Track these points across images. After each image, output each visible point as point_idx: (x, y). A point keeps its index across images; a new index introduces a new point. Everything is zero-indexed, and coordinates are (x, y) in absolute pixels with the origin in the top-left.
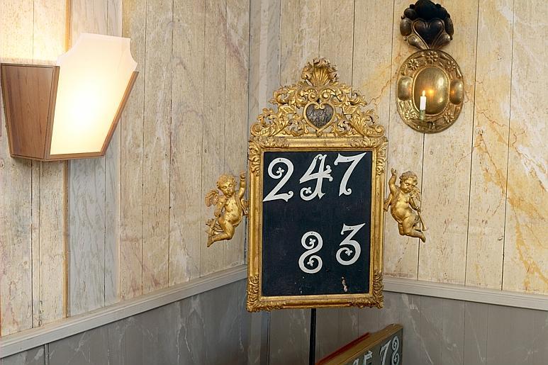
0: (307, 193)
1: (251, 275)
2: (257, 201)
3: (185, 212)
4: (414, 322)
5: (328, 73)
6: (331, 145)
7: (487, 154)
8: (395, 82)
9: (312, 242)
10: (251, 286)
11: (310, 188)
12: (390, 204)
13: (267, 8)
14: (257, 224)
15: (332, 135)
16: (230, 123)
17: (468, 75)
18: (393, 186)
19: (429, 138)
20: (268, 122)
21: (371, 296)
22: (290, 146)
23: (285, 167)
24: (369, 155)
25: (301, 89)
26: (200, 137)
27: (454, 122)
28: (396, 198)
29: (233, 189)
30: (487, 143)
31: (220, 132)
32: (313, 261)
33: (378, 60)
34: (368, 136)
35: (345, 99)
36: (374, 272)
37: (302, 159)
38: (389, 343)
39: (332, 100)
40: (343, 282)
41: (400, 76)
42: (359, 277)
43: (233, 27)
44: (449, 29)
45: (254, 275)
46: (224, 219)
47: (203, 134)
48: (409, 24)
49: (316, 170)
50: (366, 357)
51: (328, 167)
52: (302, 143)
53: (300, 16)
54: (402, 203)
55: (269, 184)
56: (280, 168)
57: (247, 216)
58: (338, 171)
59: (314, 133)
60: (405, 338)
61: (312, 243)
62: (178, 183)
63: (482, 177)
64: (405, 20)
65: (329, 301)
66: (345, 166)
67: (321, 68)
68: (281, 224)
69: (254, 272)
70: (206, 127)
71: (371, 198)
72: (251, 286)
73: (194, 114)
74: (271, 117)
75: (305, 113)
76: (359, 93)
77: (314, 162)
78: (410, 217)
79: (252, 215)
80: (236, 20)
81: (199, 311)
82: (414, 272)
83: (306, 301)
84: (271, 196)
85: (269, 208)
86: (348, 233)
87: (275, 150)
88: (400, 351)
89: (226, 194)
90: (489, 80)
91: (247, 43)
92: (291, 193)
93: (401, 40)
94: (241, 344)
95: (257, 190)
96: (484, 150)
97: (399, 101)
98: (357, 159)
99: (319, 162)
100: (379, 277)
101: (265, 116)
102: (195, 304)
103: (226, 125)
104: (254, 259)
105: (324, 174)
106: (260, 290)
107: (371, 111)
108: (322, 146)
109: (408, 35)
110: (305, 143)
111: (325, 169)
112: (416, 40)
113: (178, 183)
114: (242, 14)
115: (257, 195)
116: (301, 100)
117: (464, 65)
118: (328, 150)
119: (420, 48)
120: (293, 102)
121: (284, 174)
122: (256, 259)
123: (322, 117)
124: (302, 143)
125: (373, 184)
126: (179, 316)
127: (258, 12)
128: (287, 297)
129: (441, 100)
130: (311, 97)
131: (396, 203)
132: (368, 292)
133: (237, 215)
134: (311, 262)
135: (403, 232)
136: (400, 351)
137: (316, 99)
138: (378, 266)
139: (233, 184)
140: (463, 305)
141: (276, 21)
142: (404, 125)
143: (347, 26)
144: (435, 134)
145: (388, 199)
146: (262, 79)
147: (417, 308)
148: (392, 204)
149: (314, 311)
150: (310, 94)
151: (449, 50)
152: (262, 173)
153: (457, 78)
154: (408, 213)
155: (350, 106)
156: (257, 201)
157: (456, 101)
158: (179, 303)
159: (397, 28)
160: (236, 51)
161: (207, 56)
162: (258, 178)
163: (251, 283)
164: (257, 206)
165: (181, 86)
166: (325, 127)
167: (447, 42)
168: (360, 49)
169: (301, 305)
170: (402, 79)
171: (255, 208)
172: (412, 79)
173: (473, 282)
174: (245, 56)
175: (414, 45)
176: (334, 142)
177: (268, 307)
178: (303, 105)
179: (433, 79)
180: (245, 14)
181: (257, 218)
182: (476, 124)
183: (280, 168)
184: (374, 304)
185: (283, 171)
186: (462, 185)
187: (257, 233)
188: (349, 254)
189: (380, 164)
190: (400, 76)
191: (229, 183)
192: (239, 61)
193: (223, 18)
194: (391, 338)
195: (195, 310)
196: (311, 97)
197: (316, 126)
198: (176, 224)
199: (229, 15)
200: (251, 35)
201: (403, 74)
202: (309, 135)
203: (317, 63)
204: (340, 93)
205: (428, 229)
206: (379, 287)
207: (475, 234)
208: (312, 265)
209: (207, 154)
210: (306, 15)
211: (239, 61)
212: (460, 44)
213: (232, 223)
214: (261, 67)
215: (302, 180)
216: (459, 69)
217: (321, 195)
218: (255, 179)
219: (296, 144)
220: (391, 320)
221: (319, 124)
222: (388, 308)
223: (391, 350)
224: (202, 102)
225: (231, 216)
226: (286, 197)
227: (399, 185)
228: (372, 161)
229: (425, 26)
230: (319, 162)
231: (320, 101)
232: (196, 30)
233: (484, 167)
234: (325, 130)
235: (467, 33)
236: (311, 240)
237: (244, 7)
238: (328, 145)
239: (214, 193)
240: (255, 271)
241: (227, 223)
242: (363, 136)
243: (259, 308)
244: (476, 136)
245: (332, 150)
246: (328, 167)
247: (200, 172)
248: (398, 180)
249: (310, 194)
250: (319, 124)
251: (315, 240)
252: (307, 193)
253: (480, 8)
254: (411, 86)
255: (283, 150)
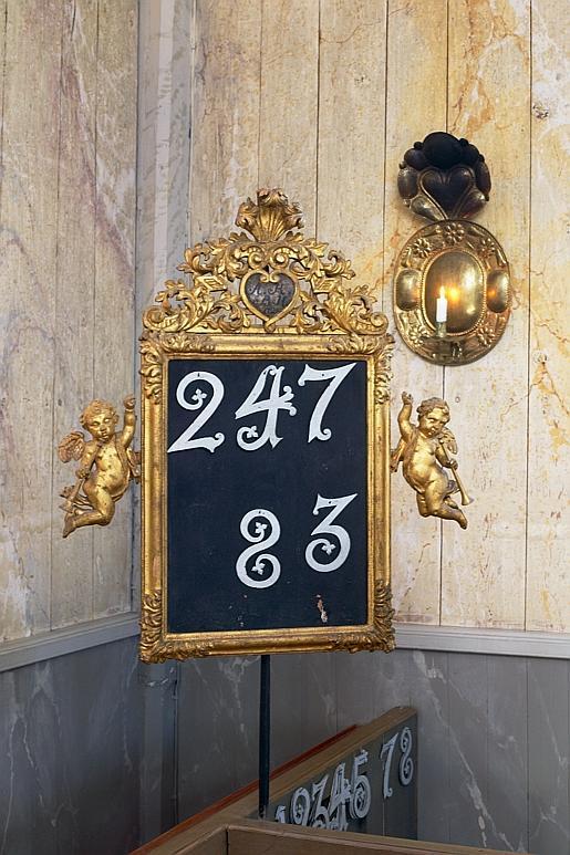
0: (249, 436)
1: (147, 592)
2: (157, 451)
3: (22, 508)
4: (437, 701)
5: (285, 217)
6: (292, 348)
7: (555, 396)
8: (390, 280)
9: (261, 528)
10: (146, 614)
11: (254, 428)
12: (402, 459)
13: (167, 161)
14: (157, 494)
15: (293, 331)
16: (102, 358)
17: (516, 262)
18: (405, 424)
19: (452, 373)
20: (175, 306)
21: (372, 628)
22: (217, 349)
23: (208, 389)
24: (360, 369)
25: (236, 247)
26: (50, 376)
27: (496, 342)
28: (412, 447)
29: (112, 428)
30: (554, 378)
31: (86, 370)
32: (263, 565)
33: (359, 244)
34: (359, 334)
35: (315, 267)
36: (377, 583)
37: (239, 374)
38: (393, 740)
39: (292, 267)
40: (320, 605)
41: (400, 269)
42: (352, 593)
43: (107, 191)
44: (483, 183)
45: (153, 591)
46: (94, 484)
47: (55, 372)
48: (413, 179)
49: (265, 395)
50: (358, 761)
51: (287, 389)
52: (239, 343)
53: (223, 176)
54: (422, 460)
55: (178, 420)
56: (198, 391)
57: (139, 479)
58: (306, 397)
59: (259, 327)
60: (421, 730)
61: (261, 531)
62: (9, 455)
63: (547, 436)
64: (405, 172)
65: (294, 639)
66: (319, 387)
67: (273, 206)
68: (204, 497)
69: (152, 585)
70: (61, 359)
71: (366, 445)
72: (146, 614)
73: (39, 334)
74: (181, 296)
75: (243, 290)
76: (339, 255)
77: (263, 377)
78: (436, 484)
79: (147, 477)
80: (112, 180)
81: (49, 691)
82: (435, 612)
83: (252, 641)
84: (183, 443)
85: (179, 466)
86: (325, 511)
87: (188, 356)
88: (414, 755)
89: (97, 437)
90: (555, 269)
91: (132, 222)
92: (221, 437)
93: (399, 208)
94: (126, 756)
95: (156, 430)
96: (550, 389)
97: (398, 311)
98: (339, 374)
99: (270, 379)
100: (385, 592)
101: (171, 293)
102: (42, 679)
103: (97, 361)
104: (152, 560)
105: (280, 401)
106: (165, 621)
107: (363, 289)
108: (276, 349)
109: (411, 197)
110: (244, 343)
111: (282, 393)
112: (426, 206)
113: (9, 455)
114: (124, 171)
115: (156, 439)
116: (235, 266)
117: (511, 245)
118: (287, 357)
119: (432, 218)
120: (221, 269)
121: (206, 402)
122: (157, 560)
123: (275, 297)
124: (239, 343)
125: (370, 421)
126: (13, 699)
127: (152, 168)
128: (216, 633)
129: (471, 310)
130: (254, 261)
131: (412, 456)
132: (366, 623)
133: (120, 477)
134: (259, 567)
135: (426, 511)
136: (414, 755)
137: (263, 265)
138: (384, 573)
139: (113, 418)
140: (523, 665)
141: (183, 185)
142: (409, 354)
143: (306, 188)
144: (462, 367)
145: (398, 449)
146: (159, 284)
147: (441, 676)
148: (404, 459)
149: (265, 658)
150: (252, 255)
151: (485, 219)
152: (165, 399)
153: (498, 267)
154: (434, 475)
155: (325, 279)
156: (157, 451)
157: (498, 306)
158: (11, 674)
159: (392, 188)
160: (113, 233)
161: (63, 234)
162: (157, 408)
163: (147, 607)
164: (157, 460)
165: (15, 282)
166: (279, 315)
167: (479, 206)
168: (328, 227)
169: (241, 648)
170: (403, 273)
171: (153, 465)
172: (420, 273)
173: (538, 623)
174: (129, 244)
175: (423, 213)
176: (296, 343)
177: (180, 652)
178: (240, 275)
179: (456, 271)
180: (128, 173)
181: (155, 483)
182: (534, 344)
183: (198, 391)
184: (378, 644)
185: (204, 396)
186: (513, 454)
187: (157, 512)
188: (329, 552)
189: (382, 383)
190: (400, 269)
191: (103, 416)
192: (118, 250)
193: (90, 174)
194: (398, 729)
195: (42, 690)
196: (254, 261)
197: (264, 313)
198: (6, 529)
199: (101, 171)
200: (139, 207)
201: (405, 266)
202: (251, 330)
203: (265, 197)
204: (306, 254)
205: (472, 501)
206: (385, 613)
207: (539, 538)
208: (261, 572)
209: (62, 408)
210: (234, 173)
211: (118, 250)
212: (500, 211)
213: (111, 494)
214: (156, 263)
215: (241, 413)
216: (502, 251)
217: (275, 441)
218: (152, 411)
219: (227, 345)
220: (396, 700)
221: (269, 310)
222: (390, 678)
223: (399, 753)
224: (53, 314)
225: (108, 478)
226: (210, 444)
227: (418, 424)
228: (366, 379)
229: (440, 179)
230: (270, 379)
231: (270, 269)
232: (43, 188)
233: (551, 418)
234: (280, 321)
235: (512, 191)
236: (258, 524)
237: (127, 160)
238: (287, 348)
239: (75, 438)
240: (154, 580)
241: (101, 491)
242: (350, 334)
243: (163, 656)
244: (535, 366)
245: (294, 357)
246: (287, 389)
247: (49, 438)
248: (415, 415)
249: (256, 439)
250: (269, 310)
251: (265, 526)
252: (249, 436)
253: (533, 147)
254: (418, 284)
255: (204, 357)
